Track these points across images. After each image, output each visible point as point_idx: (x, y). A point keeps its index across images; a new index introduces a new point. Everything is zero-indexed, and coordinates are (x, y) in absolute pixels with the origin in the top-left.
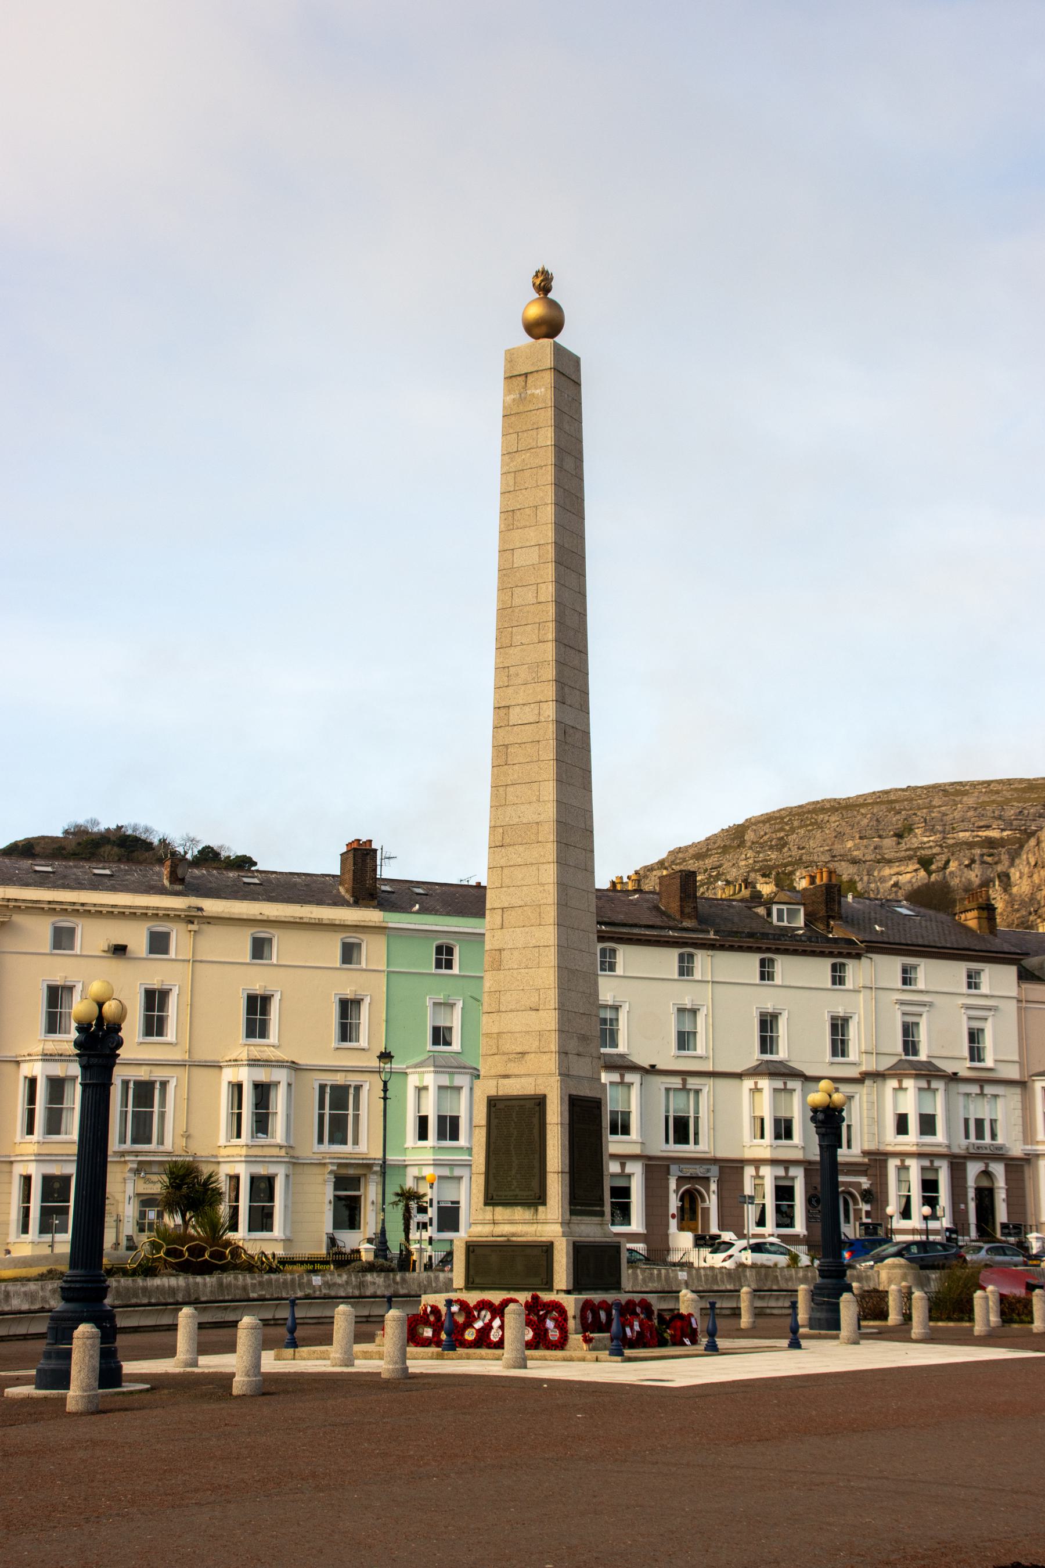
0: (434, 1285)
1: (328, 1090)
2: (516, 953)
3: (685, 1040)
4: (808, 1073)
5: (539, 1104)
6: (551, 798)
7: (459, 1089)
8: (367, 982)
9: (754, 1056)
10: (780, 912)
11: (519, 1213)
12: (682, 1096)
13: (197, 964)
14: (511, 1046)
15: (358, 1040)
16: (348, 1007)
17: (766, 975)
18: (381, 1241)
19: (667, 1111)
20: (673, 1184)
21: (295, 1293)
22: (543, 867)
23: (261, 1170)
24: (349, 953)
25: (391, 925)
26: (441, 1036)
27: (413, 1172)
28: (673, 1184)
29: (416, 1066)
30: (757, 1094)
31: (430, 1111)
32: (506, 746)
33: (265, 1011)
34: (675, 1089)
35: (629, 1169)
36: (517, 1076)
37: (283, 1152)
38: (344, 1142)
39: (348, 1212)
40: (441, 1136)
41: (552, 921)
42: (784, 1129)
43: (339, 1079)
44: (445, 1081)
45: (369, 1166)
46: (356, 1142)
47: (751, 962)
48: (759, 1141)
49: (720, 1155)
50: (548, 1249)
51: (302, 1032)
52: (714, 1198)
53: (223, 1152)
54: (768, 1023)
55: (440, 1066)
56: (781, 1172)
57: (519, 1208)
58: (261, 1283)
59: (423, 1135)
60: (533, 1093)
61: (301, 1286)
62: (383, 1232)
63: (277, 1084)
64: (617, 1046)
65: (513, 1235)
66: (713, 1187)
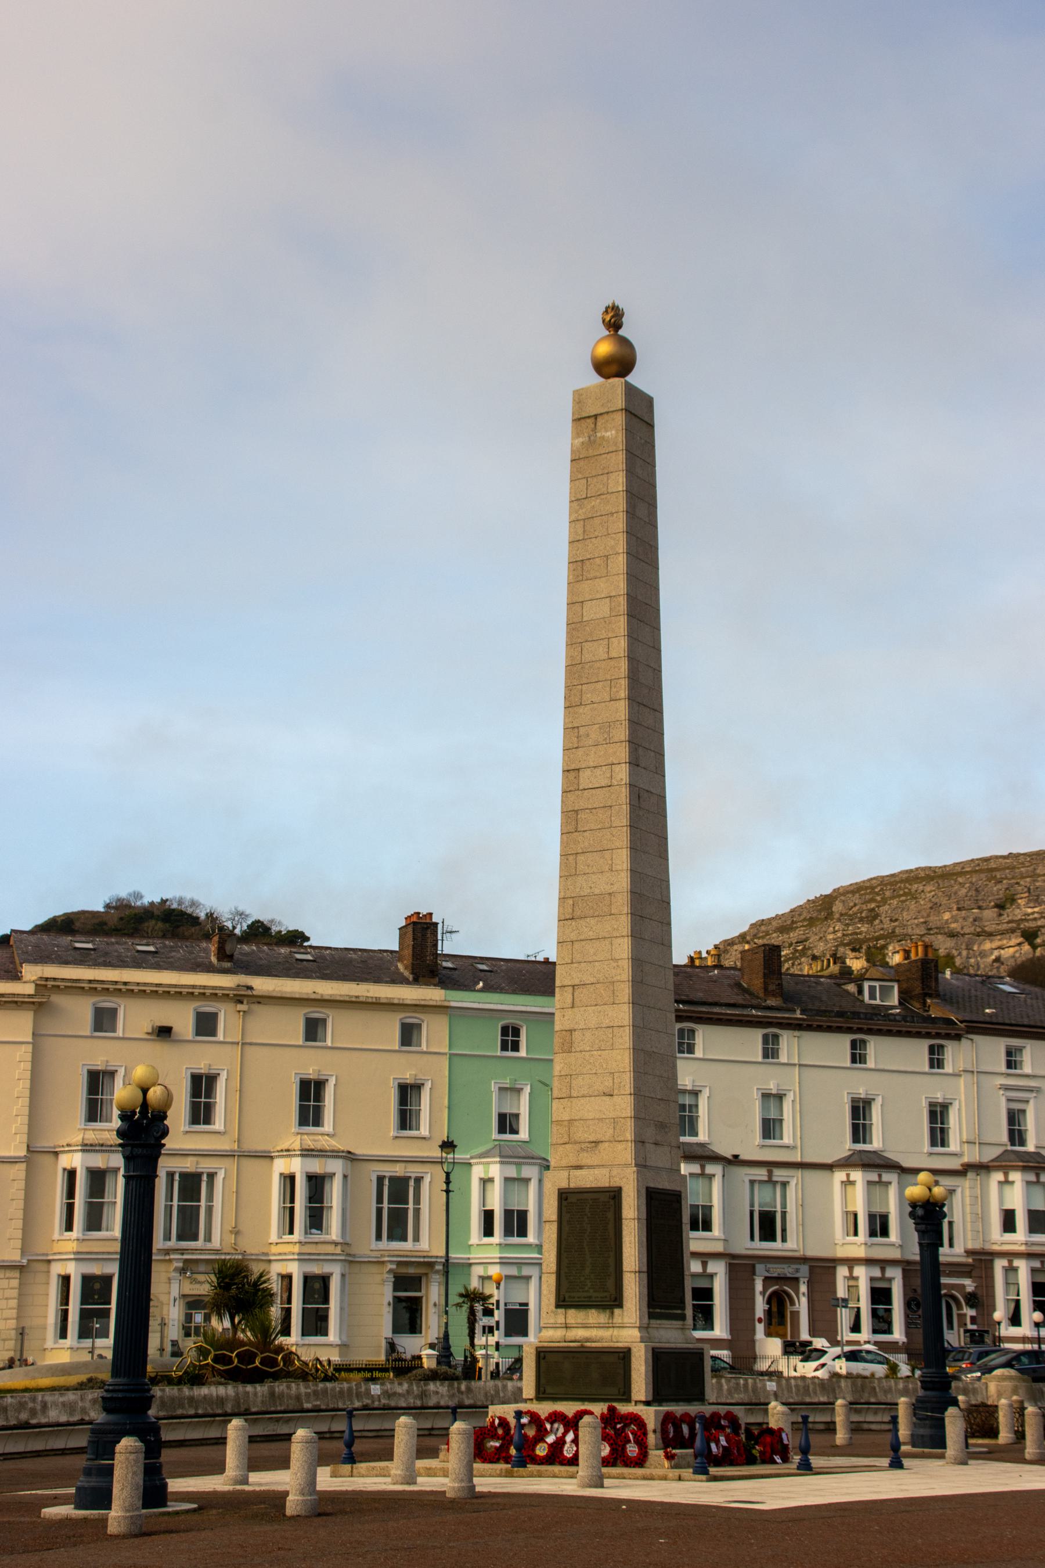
0: (501, 1395)
1: (386, 1182)
2: (588, 1034)
3: (770, 1128)
4: (905, 1164)
5: (614, 1198)
7: (527, 1181)
8: (430, 1066)
9: (846, 1146)
10: (872, 989)
11: (593, 1316)
12: (768, 1189)
14: (582, 1134)
16: (408, 1093)
18: (444, 1347)
19: (752, 1205)
20: (759, 1286)
21: (352, 1403)
23: (315, 1269)
24: (409, 1034)
25: (453, 1004)
26: (507, 1123)
27: (478, 1271)
28: (759, 1286)
29: (481, 1156)
30: (849, 1188)
31: (496, 1204)
32: (576, 812)
34: (761, 1182)
36: (590, 1167)
37: (338, 1250)
38: (404, 1238)
39: (408, 1315)
40: (508, 1232)
41: (626, 999)
42: (879, 1226)
43: (399, 1170)
44: (512, 1172)
45: (430, 1265)
46: (417, 1239)
48: (852, 1238)
49: (810, 1253)
50: (625, 1355)
52: (804, 1300)
54: (860, 1109)
55: (507, 1156)
56: (877, 1273)
57: (593, 1311)
58: (316, 1393)
59: (488, 1231)
60: (607, 1185)
61: (359, 1396)
63: (332, 1176)
64: (696, 1135)
65: (588, 1340)
66: (803, 1288)
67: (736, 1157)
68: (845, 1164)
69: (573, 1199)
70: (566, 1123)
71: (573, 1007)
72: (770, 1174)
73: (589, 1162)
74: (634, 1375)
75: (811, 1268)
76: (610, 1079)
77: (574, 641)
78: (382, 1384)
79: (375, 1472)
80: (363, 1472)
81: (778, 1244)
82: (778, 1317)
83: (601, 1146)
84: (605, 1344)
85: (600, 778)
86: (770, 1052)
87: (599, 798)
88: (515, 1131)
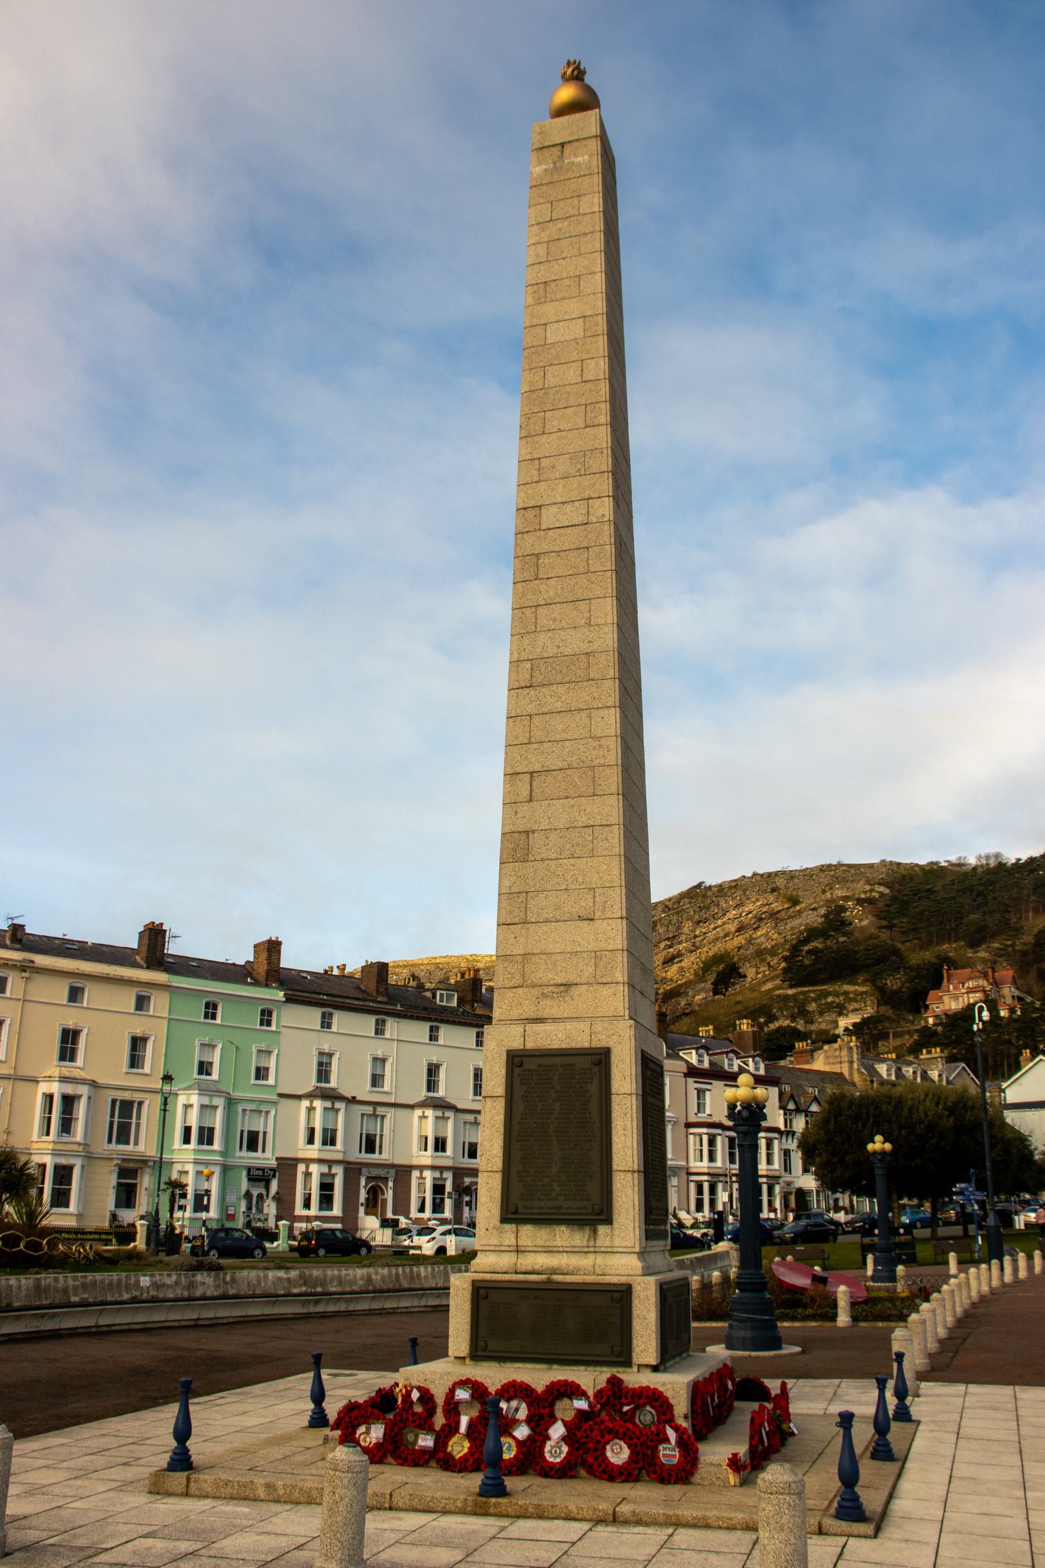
0: (263, 1284)
1: (118, 1103)
2: (554, 836)
3: (377, 1080)
4: (459, 1106)
5: (598, 1063)
6: (609, 620)
7: (216, 1107)
8: (154, 1025)
9: (423, 1094)
10: (442, 995)
11: (563, 1236)
12: (372, 1120)
13: (26, 1003)
14: (542, 973)
15: (143, 1068)
16: (137, 1043)
17: (433, 1037)
18: (153, 1219)
19: (362, 1129)
20: (363, 1182)
21: (121, 1295)
22: (597, 715)
23: (63, 1161)
24: (141, 1003)
25: (174, 984)
26: (204, 1068)
27: (177, 1167)
28: (363, 1182)
29: (185, 1089)
30: (424, 1120)
31: (193, 1122)
32: (537, 556)
33: (75, 1042)
34: (368, 1115)
35: (334, 1170)
36: (555, 1020)
37: (81, 1148)
38: (127, 1143)
39: (126, 1196)
40: (201, 1141)
41: (614, 789)
42: (440, 1145)
43: (127, 1096)
44: (206, 1101)
45: (145, 1162)
46: (136, 1143)
47: (424, 1028)
48: (423, 1153)
49: (397, 1162)
50: (621, 1296)
51: (102, 1061)
52: (391, 1192)
53: (35, 1146)
54: (433, 1070)
55: (204, 1090)
56: (437, 1175)
57: (563, 1228)
58: (84, 1286)
59: (187, 1140)
60: (586, 1045)
61: (128, 1287)
62: (157, 1212)
63: (80, 1097)
64: (329, 1082)
65: (554, 1271)
66: (391, 1184)
67: (354, 1098)
68: (311, 1096)
69: (530, 1064)
70: (519, 959)
71: (530, 800)
72: (375, 1110)
73: (555, 1012)
74: (637, 1326)
75: (397, 1171)
76: (589, 897)
77: (534, 365)
78: (152, 1276)
79: (229, 1490)
80: (208, 1488)
81: (376, 1155)
82: (373, 1205)
83: (575, 991)
84: (589, 1279)
85: (573, 514)
86: (379, 1031)
87: (571, 539)
88: (209, 1074)
